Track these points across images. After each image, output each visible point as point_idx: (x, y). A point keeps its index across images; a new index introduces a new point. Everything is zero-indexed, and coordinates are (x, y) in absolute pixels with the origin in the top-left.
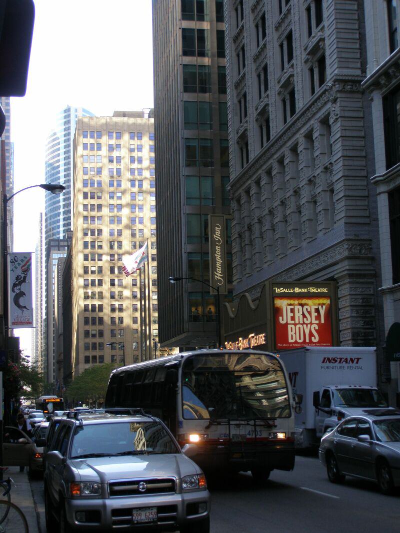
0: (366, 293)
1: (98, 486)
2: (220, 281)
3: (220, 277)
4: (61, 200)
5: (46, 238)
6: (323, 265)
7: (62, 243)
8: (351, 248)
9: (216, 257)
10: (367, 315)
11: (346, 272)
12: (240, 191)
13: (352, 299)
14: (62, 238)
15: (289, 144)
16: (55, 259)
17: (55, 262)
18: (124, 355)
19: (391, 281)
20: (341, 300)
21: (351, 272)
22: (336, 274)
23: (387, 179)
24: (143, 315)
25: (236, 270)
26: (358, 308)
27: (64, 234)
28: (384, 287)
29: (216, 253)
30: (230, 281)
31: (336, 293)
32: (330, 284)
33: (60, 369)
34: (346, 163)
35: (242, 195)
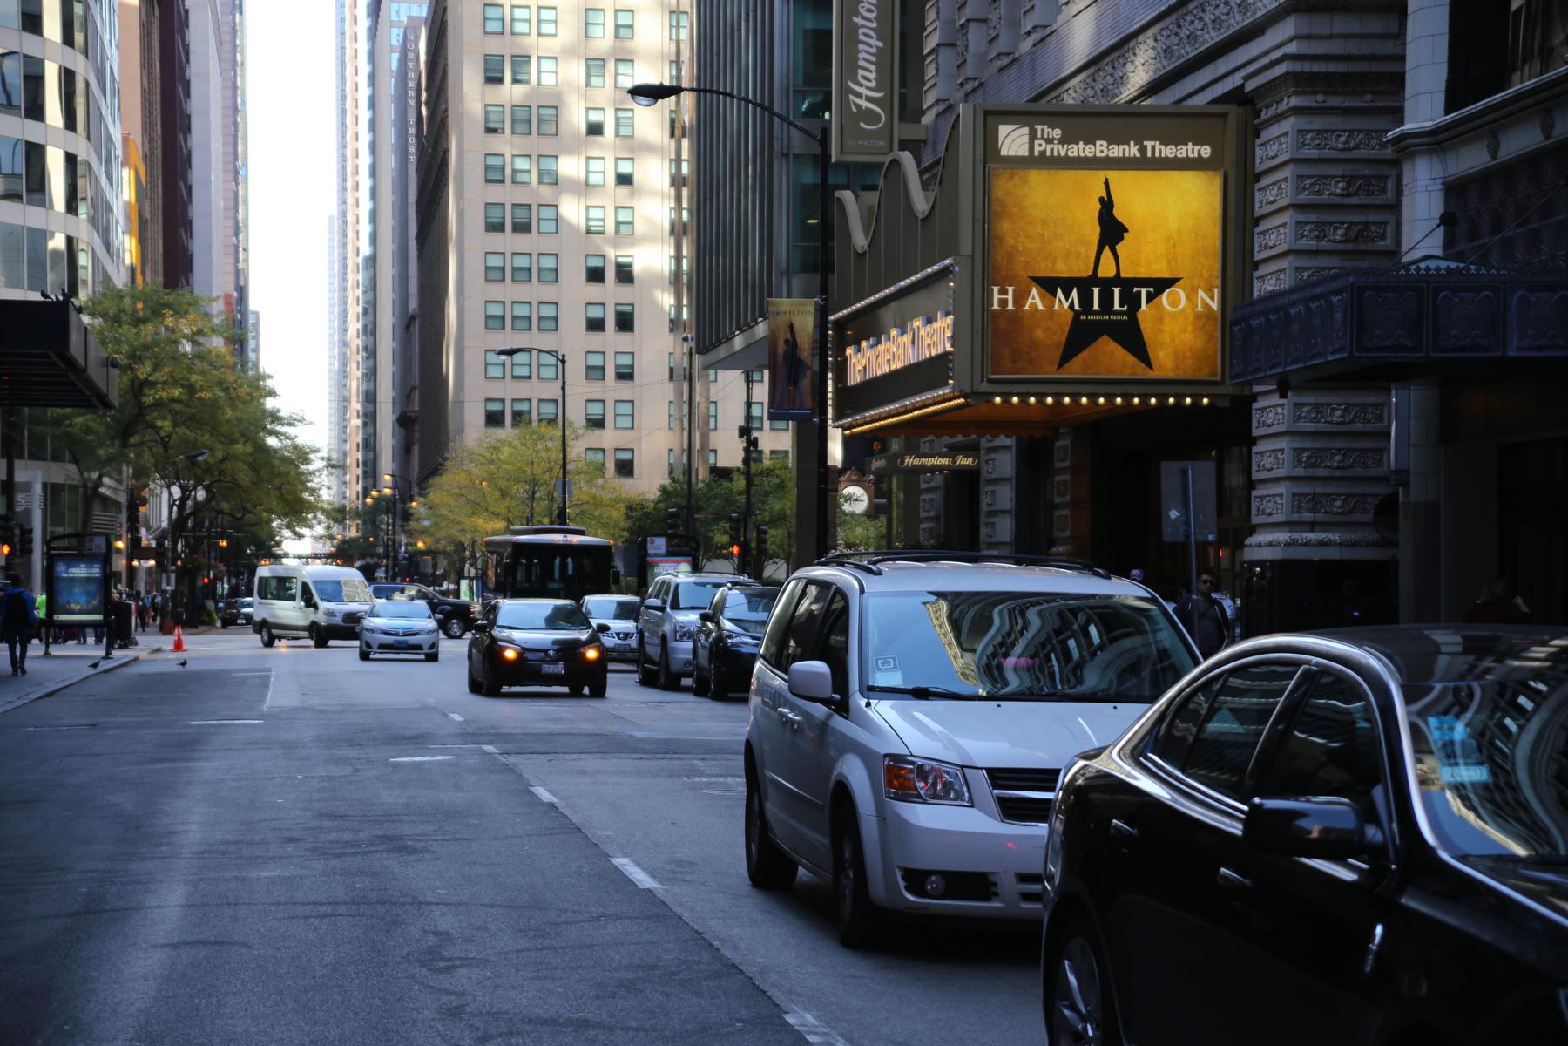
0: (1363, 153)
1: (726, 532)
2: (870, 116)
3: (869, 99)
6: (1211, 38)
9: (857, 26)
10: (1363, 247)
11: (1281, 69)
13: (1300, 177)
19: (1441, 99)
20: (1265, 181)
21: (1307, 67)
25: (933, 66)
28: (1408, 126)
29: (857, 14)
30: (909, 110)
32: (1224, 116)
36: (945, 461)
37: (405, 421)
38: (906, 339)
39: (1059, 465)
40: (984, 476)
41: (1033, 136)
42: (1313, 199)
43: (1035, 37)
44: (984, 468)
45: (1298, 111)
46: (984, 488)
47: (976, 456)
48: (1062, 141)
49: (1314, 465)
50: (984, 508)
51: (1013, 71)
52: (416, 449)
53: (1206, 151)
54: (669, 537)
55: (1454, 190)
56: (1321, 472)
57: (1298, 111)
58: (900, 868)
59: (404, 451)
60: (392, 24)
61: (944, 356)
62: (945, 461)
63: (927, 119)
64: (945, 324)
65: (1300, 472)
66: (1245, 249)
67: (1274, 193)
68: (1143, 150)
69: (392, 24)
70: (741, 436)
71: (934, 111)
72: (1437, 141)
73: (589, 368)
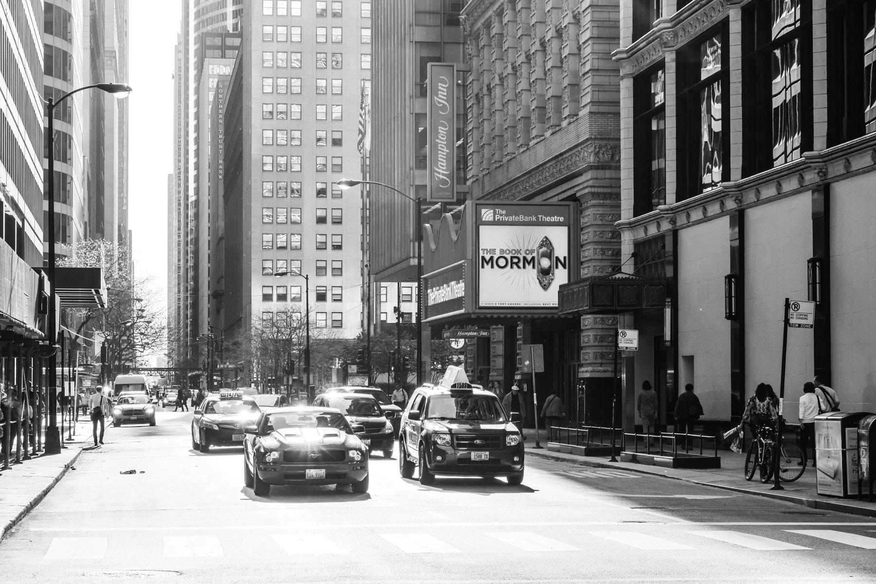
3: (443, 174)
4: (230, 16)
5: (197, 28)
7: (229, 41)
8: (598, 152)
11: (586, 191)
12: (490, 13)
14: (230, 29)
15: (482, 21)
16: (213, 76)
17: (213, 83)
18: (787, 322)
21: (596, 190)
22: (577, 191)
23: (632, 53)
24: (644, 43)
26: (604, 247)
27: (235, 21)
31: (577, 221)
32: (569, 205)
33: (218, 311)
34: (597, 16)
35: (493, 20)
36: (475, 334)
37: (216, 296)
38: (449, 289)
39: (518, 337)
40: (492, 340)
41: (495, 213)
42: (601, 240)
43: (509, 157)
44: (492, 337)
45: (594, 206)
46: (492, 346)
47: (489, 332)
48: (506, 215)
49: (602, 341)
50: (492, 354)
51: (501, 169)
52: (223, 311)
53: (562, 219)
54: (358, 364)
55: (637, 245)
56: (604, 344)
57: (594, 206)
58: (127, 98)
59: (215, 312)
60: (210, 76)
61: (460, 299)
62: (475, 334)
63: (469, 183)
64: (462, 285)
65: (597, 344)
66: (578, 257)
67: (587, 236)
68: (537, 218)
69: (210, 76)
70: (395, 312)
71: (471, 180)
72: (631, 226)
73: (318, 268)
